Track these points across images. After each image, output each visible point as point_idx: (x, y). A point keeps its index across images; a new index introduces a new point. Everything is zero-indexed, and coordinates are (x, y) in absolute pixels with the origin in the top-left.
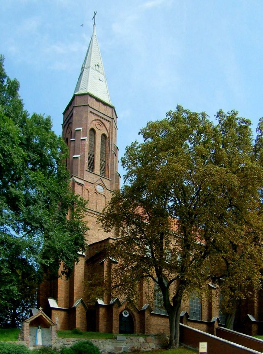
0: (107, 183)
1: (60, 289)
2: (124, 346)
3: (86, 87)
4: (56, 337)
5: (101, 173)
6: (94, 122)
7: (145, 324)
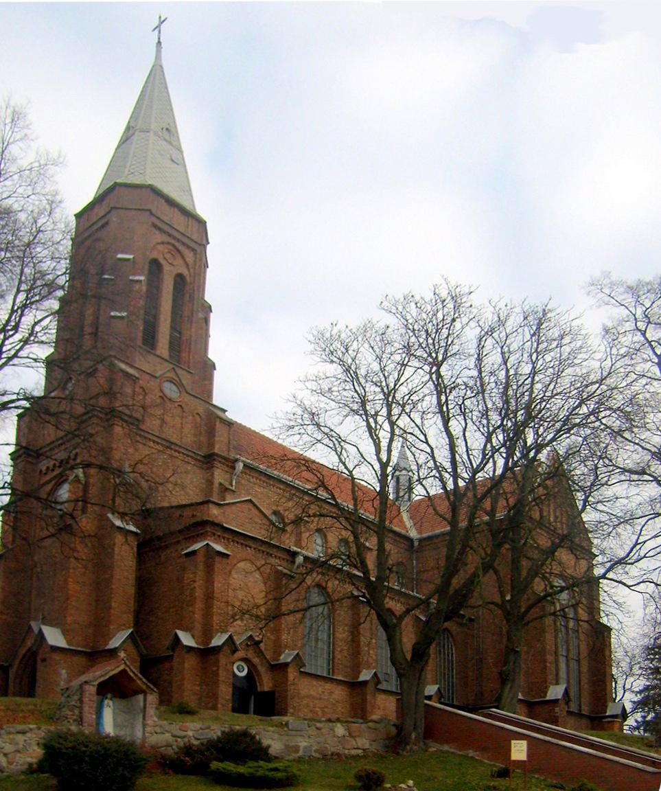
0: (186, 379)
2: (305, 744)
3: (142, 172)
4: (155, 719)
5: (170, 356)
6: (160, 247)
7: (289, 693)
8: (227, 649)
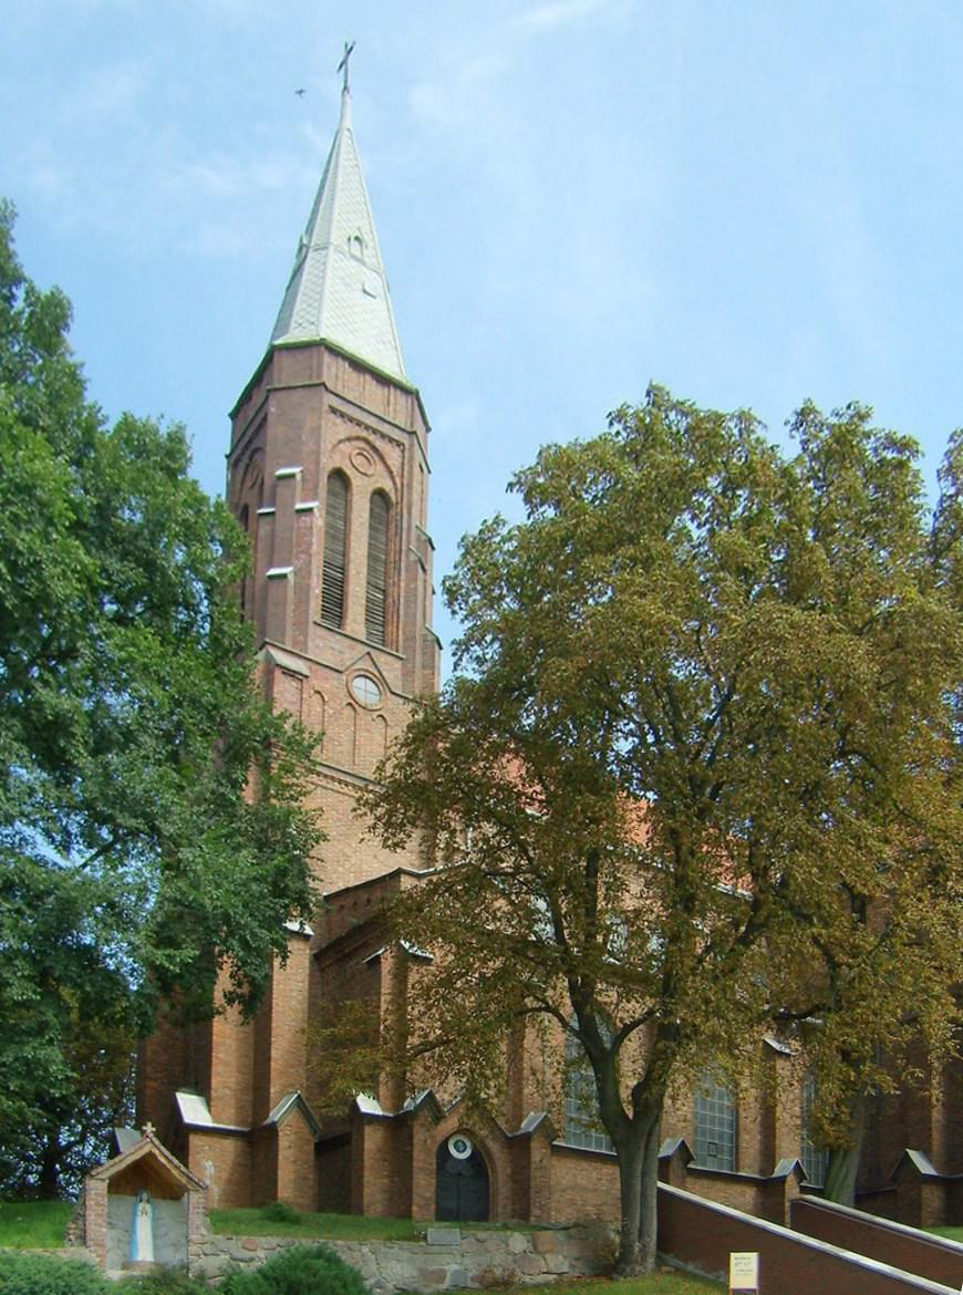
1: (221, 1056)
2: (456, 1267)
3: (313, 319)
4: (204, 1231)
5: (369, 634)
7: (532, 1184)
8: (426, 1115)
